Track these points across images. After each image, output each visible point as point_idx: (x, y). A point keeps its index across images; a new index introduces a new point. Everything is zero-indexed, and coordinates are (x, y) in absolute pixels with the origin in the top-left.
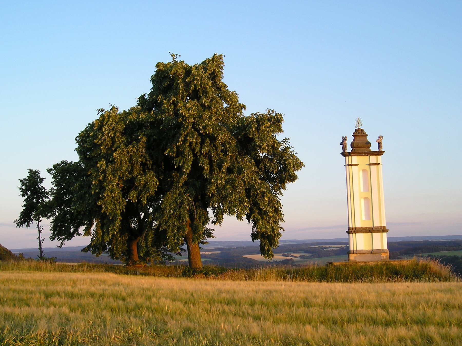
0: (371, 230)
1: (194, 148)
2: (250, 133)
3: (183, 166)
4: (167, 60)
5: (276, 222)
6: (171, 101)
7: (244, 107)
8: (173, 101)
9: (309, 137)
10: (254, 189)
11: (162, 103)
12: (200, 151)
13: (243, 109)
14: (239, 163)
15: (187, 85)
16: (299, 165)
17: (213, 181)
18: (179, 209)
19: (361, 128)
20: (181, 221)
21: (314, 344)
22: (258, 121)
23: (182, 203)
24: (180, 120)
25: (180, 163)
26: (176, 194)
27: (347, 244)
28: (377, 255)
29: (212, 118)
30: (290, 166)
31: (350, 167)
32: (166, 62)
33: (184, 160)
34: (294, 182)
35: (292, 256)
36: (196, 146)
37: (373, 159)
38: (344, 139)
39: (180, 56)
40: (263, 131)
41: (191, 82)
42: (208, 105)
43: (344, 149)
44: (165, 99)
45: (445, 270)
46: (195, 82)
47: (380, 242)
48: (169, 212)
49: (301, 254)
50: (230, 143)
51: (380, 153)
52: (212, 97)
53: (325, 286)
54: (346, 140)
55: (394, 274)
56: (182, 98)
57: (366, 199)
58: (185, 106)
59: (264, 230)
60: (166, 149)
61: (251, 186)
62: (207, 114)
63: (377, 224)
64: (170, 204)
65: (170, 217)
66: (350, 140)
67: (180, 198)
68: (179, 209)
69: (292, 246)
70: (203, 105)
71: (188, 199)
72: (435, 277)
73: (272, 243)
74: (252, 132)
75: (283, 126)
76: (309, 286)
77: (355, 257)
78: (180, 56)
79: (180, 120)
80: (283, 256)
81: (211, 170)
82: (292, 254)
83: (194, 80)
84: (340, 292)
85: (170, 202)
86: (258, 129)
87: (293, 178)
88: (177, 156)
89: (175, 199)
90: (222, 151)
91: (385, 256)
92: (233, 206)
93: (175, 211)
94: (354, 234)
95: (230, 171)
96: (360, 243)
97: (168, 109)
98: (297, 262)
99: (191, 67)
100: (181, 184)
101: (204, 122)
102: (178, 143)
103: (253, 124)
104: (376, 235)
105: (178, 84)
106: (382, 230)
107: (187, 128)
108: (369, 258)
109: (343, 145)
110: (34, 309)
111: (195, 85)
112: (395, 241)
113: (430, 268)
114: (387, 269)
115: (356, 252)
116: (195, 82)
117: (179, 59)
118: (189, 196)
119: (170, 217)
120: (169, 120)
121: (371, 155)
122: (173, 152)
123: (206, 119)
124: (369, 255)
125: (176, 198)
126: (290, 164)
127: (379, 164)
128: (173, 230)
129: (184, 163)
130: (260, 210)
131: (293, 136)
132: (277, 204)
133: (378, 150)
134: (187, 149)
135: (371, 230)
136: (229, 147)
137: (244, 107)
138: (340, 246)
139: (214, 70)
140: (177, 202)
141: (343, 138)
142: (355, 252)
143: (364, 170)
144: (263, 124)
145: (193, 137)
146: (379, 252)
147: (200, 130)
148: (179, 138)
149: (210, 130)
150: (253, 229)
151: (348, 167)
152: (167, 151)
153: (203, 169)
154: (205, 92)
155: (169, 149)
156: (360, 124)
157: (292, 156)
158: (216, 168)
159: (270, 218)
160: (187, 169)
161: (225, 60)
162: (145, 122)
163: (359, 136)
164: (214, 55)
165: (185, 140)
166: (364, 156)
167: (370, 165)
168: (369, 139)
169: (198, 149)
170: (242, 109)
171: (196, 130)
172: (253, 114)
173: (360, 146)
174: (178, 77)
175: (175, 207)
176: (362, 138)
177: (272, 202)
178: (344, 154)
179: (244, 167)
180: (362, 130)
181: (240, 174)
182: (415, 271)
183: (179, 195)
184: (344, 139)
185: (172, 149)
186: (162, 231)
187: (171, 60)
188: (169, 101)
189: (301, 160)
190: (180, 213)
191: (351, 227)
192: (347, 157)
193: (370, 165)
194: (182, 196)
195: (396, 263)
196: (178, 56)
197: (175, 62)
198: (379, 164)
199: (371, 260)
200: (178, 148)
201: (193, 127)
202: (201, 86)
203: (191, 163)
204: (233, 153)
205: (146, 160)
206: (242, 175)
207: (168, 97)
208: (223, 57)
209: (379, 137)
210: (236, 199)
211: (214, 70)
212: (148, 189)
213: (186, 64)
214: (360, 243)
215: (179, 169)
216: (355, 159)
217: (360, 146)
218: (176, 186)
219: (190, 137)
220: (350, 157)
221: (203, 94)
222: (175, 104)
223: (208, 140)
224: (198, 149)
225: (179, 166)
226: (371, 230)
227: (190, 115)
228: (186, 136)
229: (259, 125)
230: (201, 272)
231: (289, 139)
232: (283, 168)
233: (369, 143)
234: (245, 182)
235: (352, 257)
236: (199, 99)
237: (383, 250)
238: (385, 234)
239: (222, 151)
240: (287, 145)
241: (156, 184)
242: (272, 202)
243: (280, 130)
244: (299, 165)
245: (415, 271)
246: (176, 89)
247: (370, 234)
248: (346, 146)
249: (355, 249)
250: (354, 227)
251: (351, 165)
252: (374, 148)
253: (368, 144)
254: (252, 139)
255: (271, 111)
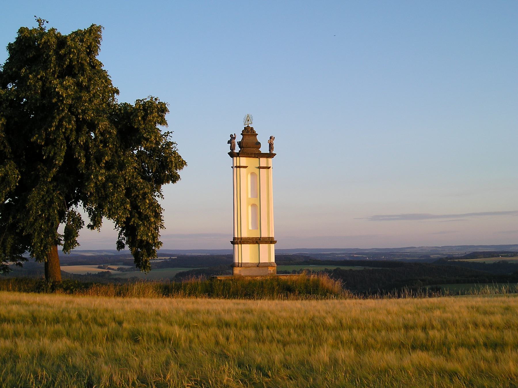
0: (259, 241)
1: (68, 136)
2: (135, 123)
3: (54, 157)
4: (32, 25)
5: (156, 229)
6: (39, 76)
7: (117, 92)
8: (41, 76)
9: (194, 133)
10: (136, 189)
11: (26, 77)
12: (77, 140)
13: (115, 94)
14: (119, 157)
15: (60, 58)
16: (182, 164)
17: (92, 176)
18: (48, 210)
19: (251, 126)
20: (50, 224)
21: (445, 386)
22: (145, 110)
23: (52, 202)
24: (54, 100)
25: (50, 152)
26: (43, 191)
27: (231, 257)
28: (263, 268)
29: (93, 101)
30: (172, 164)
31: (238, 169)
32: (30, 28)
33: (55, 150)
34: (175, 184)
35: (109, 268)
36: (71, 133)
37: (263, 162)
38: (233, 138)
39: (47, 22)
40: (150, 121)
41: (65, 55)
42: (85, 86)
43: (232, 148)
44: (30, 73)
45: (337, 285)
46: (71, 56)
47: (268, 254)
48: (35, 212)
49: (120, 266)
50: (110, 133)
51: (270, 155)
52: (89, 76)
53: (46, 298)
54: (235, 138)
55: (287, 290)
56: (52, 74)
57: (254, 205)
58: (61, 83)
59: (145, 238)
60: (33, 136)
61: (132, 185)
62: (85, 96)
63: (264, 235)
64: (37, 204)
65: (36, 220)
66: (239, 138)
67: (48, 196)
68: (48, 210)
69: (110, 257)
70: (79, 85)
71: (59, 198)
72: (324, 293)
73: (150, 254)
74: (138, 122)
75: (167, 117)
76: (171, 303)
77: (240, 271)
78: (47, 22)
79: (54, 100)
80: (99, 268)
81: (88, 163)
82: (109, 266)
83: (70, 52)
84: (299, 311)
85: (36, 201)
86: (144, 118)
87: (175, 178)
88: (46, 145)
89: (43, 198)
90: (101, 142)
91: (271, 270)
92: (115, 208)
93: (43, 211)
94: (240, 245)
95: (109, 166)
96: (246, 255)
97: (35, 86)
98: (115, 275)
99: (66, 37)
100: (49, 180)
101: (83, 105)
102: (51, 128)
103: (138, 112)
104: (263, 247)
105: (48, 56)
106: (270, 241)
107: (63, 110)
108: (255, 272)
109: (231, 143)
110: (46, 341)
111: (70, 59)
112: (224, 254)
113: (322, 284)
114: (279, 285)
115: (241, 265)
116: (71, 56)
117: (47, 27)
118: (60, 194)
119: (36, 220)
120: (36, 100)
121: (262, 157)
122: (42, 139)
123: (85, 101)
124: (255, 268)
125: (43, 196)
126: (171, 161)
127: (269, 168)
128: (39, 234)
129: (55, 154)
130: (140, 213)
131: (179, 131)
132: (158, 208)
133: (269, 152)
134: (62, 136)
135: (258, 241)
136: (109, 138)
137: (117, 92)
138: (163, 258)
139: (91, 43)
140: (44, 201)
141: (231, 136)
142: (240, 265)
143: (252, 174)
144: (152, 113)
145: (69, 122)
146: (266, 265)
147: (79, 114)
148: (52, 122)
149: (90, 115)
150: (119, 237)
151: (235, 169)
152: (35, 138)
153: (78, 161)
154: (82, 70)
155: (37, 135)
156: (250, 122)
157: (175, 154)
158: (94, 162)
159: (150, 224)
160: (59, 161)
161: (104, 34)
162: (4, 100)
163: (249, 135)
164: (92, 26)
165: (58, 127)
166: (254, 157)
167: (260, 168)
168: (259, 138)
169: (73, 138)
170: (114, 94)
171: (73, 113)
172: (139, 100)
173: (247, 145)
174: (49, 48)
175: (42, 207)
176: (252, 138)
177: (152, 205)
178: (232, 154)
179: (127, 163)
180: (252, 128)
181: (122, 171)
182: (306, 287)
183: (47, 193)
184: (233, 138)
185: (40, 135)
186: (25, 235)
187: (36, 26)
188: (36, 76)
189: (184, 158)
190: (49, 215)
191: (236, 236)
192: (235, 158)
193: (260, 168)
194: (51, 194)
195: (283, 277)
196: (45, 22)
197: (42, 29)
198: (269, 168)
199: (258, 275)
200: (48, 134)
201: (69, 110)
202: (78, 61)
203: (64, 154)
204: (114, 144)
205: (5, 147)
206: (123, 172)
207: (34, 71)
208: (102, 29)
209: (271, 138)
210: (117, 200)
211: (91, 43)
212: (9, 183)
213: (59, 33)
214: (246, 255)
215: (49, 163)
216: (243, 161)
217: (247, 145)
218: (44, 181)
219: (66, 122)
220: (238, 158)
221: (79, 71)
222: (44, 80)
223: (85, 127)
224: (73, 138)
225: (48, 156)
226: (258, 241)
227: (68, 96)
228: (61, 121)
229: (146, 115)
230: (61, 286)
231: (171, 133)
232: (165, 166)
233: (259, 144)
234: (125, 180)
235: (237, 271)
236: (74, 76)
237: (270, 263)
238: (273, 246)
239: (101, 142)
240: (169, 140)
241: (18, 177)
242: (152, 205)
243: (163, 122)
244: (182, 164)
245: (306, 287)
246: (45, 62)
247: (257, 245)
248: (234, 145)
249: (240, 262)
250: (239, 237)
251: (240, 167)
252: (264, 149)
253: (258, 144)
254: (138, 129)
255: (154, 99)
